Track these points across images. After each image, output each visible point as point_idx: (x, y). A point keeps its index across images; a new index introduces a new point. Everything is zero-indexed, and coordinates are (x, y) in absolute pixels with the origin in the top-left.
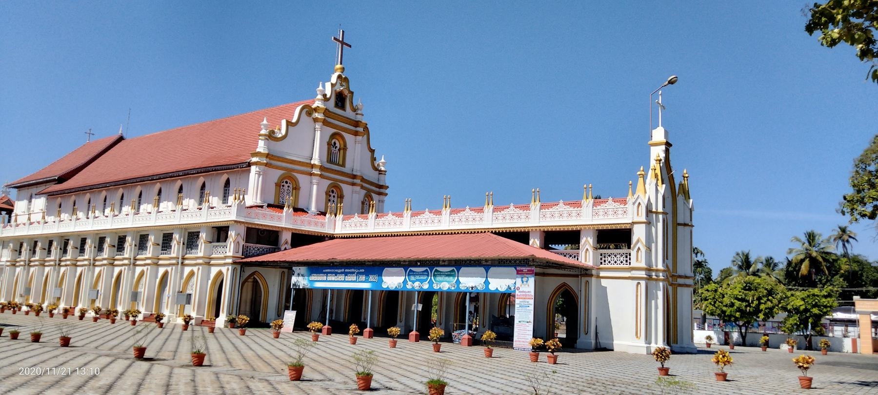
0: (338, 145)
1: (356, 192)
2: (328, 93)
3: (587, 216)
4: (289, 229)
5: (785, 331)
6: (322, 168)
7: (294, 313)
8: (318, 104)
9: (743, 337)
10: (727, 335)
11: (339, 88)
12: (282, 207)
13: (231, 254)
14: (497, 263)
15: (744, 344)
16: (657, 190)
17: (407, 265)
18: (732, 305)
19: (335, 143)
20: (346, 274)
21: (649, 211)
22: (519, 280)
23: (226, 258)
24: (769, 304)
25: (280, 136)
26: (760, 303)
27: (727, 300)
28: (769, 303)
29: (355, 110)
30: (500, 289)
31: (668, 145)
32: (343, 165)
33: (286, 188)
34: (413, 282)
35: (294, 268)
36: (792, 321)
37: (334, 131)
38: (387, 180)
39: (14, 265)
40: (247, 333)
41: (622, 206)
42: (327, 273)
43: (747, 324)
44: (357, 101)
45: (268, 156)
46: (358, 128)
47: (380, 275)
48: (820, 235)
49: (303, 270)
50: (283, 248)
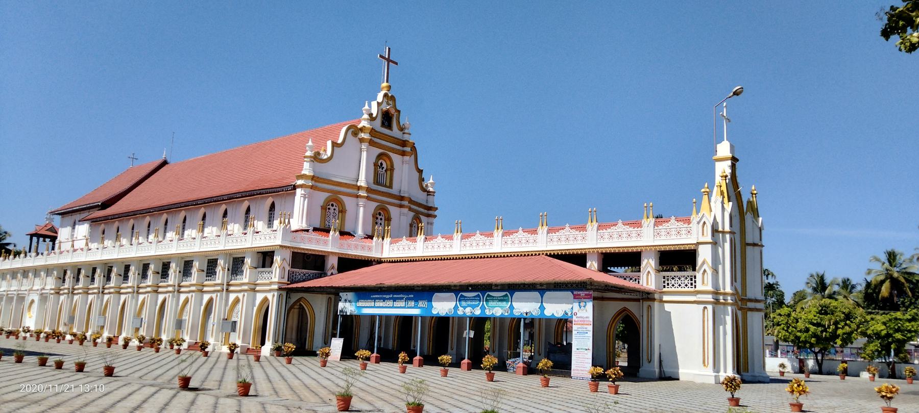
0: (384, 165)
1: (404, 214)
2: (374, 111)
3: (648, 237)
4: (335, 253)
5: (865, 358)
6: (368, 190)
7: (342, 340)
8: (364, 123)
9: (819, 364)
10: (802, 362)
11: (385, 107)
12: (328, 231)
13: (276, 280)
14: (552, 287)
15: (820, 372)
16: (723, 208)
17: (457, 290)
18: (807, 330)
19: (381, 164)
20: (395, 300)
21: (715, 231)
22: (576, 305)
23: (271, 283)
24: (847, 329)
25: (325, 157)
26: (837, 328)
27: (800, 325)
28: (847, 328)
29: (402, 129)
30: (556, 315)
31: (734, 160)
32: (391, 187)
33: (332, 211)
34: (465, 308)
35: (341, 294)
36: (871, 347)
37: (381, 151)
38: (436, 201)
39: (58, 293)
40: (293, 361)
41: (686, 225)
42: (375, 299)
43: (823, 351)
44: (404, 120)
45: (313, 178)
46: (406, 147)
47: (430, 300)
48: (902, 254)
49: (350, 295)
50: (329, 273)
